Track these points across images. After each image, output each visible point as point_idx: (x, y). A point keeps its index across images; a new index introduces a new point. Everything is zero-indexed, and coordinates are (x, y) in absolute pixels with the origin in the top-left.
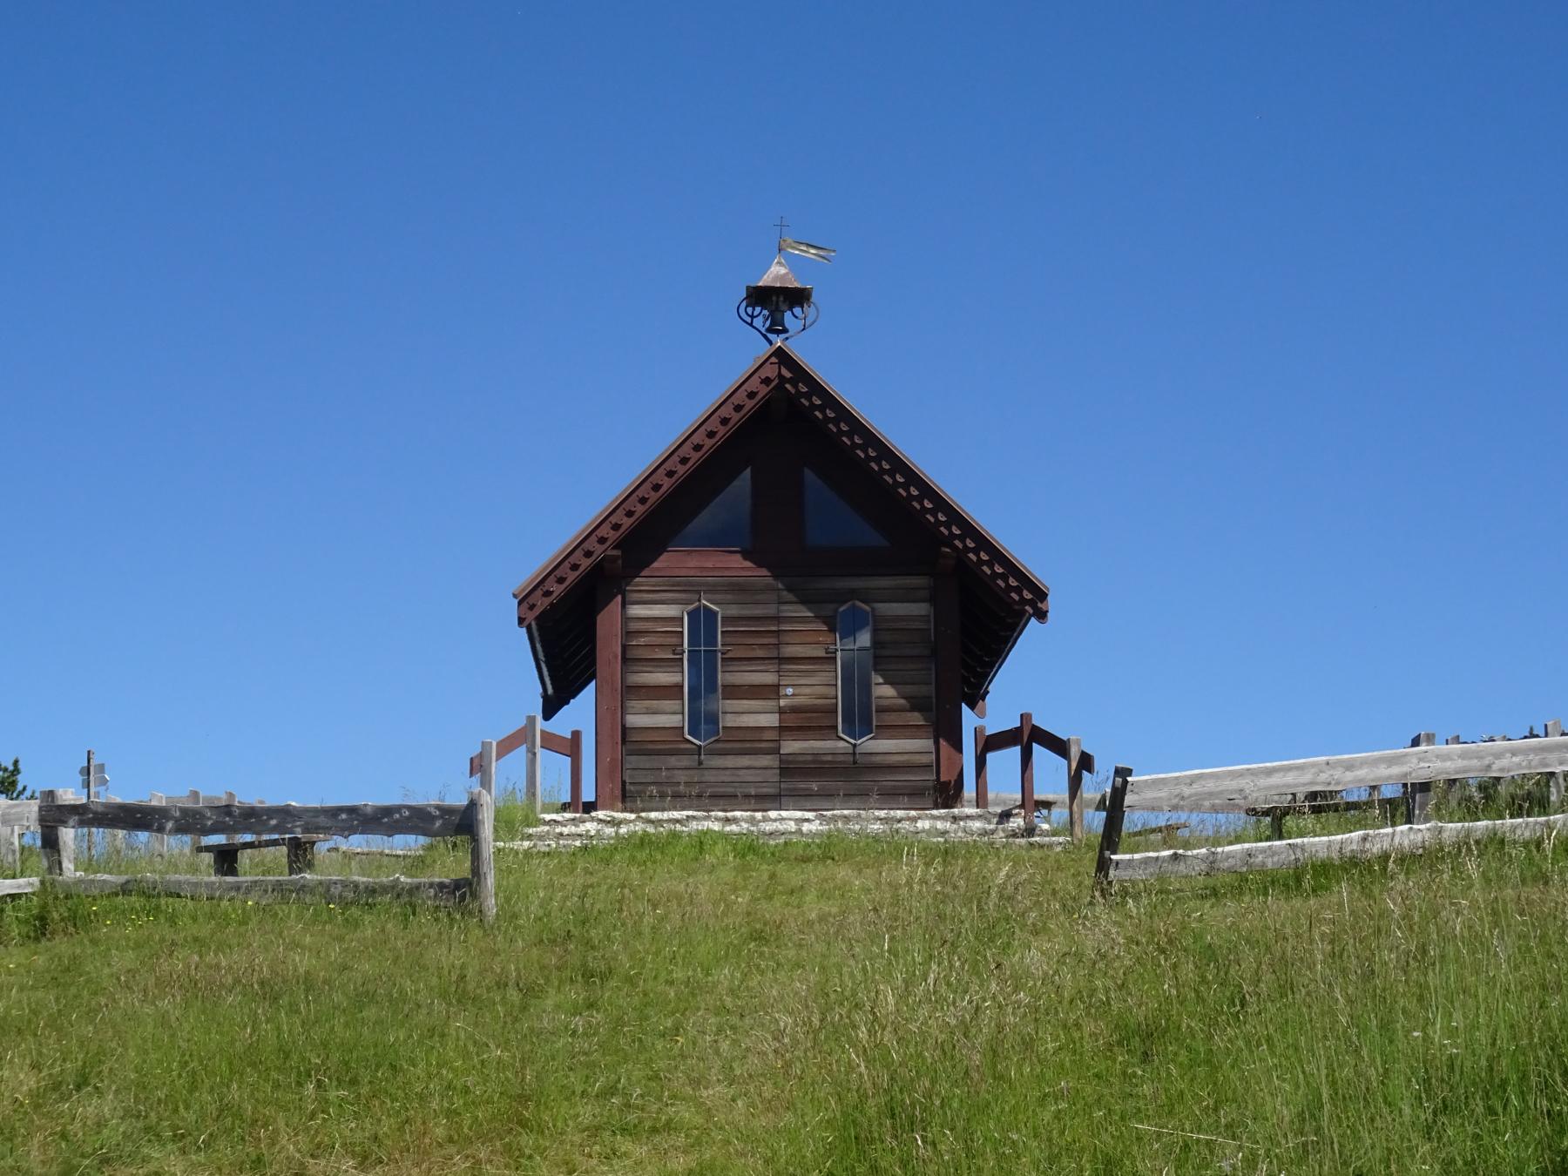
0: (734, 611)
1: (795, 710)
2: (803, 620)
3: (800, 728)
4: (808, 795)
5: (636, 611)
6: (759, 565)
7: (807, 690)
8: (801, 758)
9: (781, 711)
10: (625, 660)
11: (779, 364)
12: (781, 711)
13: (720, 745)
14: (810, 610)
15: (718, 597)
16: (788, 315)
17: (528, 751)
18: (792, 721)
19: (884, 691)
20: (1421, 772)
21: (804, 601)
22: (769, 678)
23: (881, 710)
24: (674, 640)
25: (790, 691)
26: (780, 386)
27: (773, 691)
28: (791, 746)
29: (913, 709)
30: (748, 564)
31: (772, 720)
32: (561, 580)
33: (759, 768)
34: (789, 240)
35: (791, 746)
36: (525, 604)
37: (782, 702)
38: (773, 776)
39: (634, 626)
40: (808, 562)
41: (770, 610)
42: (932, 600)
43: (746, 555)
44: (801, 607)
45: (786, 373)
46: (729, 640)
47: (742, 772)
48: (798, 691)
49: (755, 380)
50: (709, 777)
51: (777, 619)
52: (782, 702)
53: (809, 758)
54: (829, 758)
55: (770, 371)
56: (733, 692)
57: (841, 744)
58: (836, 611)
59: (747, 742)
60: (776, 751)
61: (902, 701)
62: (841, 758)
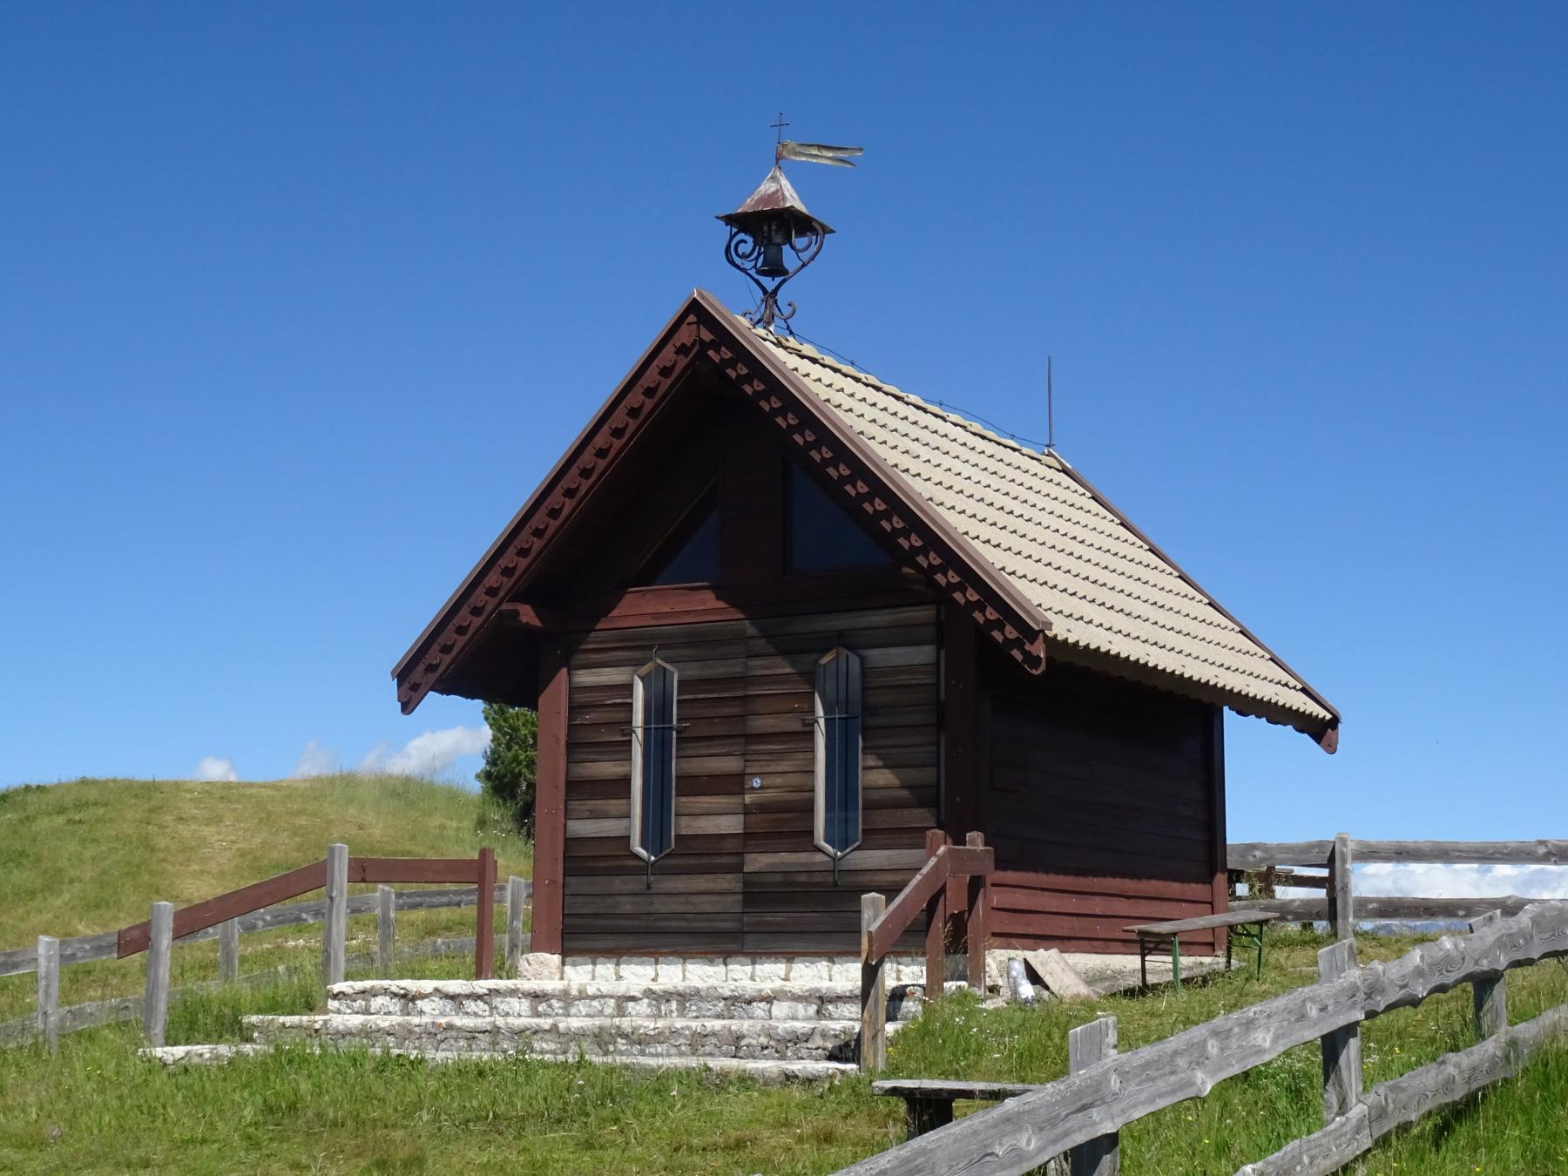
0: (694, 671)
1: (762, 808)
3: (768, 835)
4: (800, 933)
5: (585, 678)
6: (733, 603)
7: (779, 781)
8: (769, 879)
9: (747, 811)
10: (572, 746)
11: (698, 323)
12: (747, 811)
13: (673, 861)
14: (792, 664)
15: (674, 653)
16: (786, 248)
17: (1257, 724)
18: (760, 822)
19: (876, 777)
21: (785, 652)
22: (731, 764)
24: (621, 716)
25: (757, 782)
26: (702, 355)
27: (732, 784)
28: (757, 862)
29: (921, 805)
30: (722, 605)
31: (731, 824)
32: (446, 649)
33: (714, 892)
34: (791, 144)
35: (757, 862)
36: (406, 685)
37: (748, 799)
38: (733, 904)
39: (581, 698)
42: (939, 643)
43: (720, 591)
44: (778, 660)
45: (707, 336)
47: (695, 899)
48: (771, 780)
49: (669, 350)
50: (661, 905)
51: (743, 680)
52: (748, 799)
53: (778, 878)
54: (804, 878)
55: (685, 336)
56: (694, 785)
57: (819, 857)
58: (816, 662)
59: (704, 854)
60: (737, 869)
61: (905, 793)
62: (818, 878)
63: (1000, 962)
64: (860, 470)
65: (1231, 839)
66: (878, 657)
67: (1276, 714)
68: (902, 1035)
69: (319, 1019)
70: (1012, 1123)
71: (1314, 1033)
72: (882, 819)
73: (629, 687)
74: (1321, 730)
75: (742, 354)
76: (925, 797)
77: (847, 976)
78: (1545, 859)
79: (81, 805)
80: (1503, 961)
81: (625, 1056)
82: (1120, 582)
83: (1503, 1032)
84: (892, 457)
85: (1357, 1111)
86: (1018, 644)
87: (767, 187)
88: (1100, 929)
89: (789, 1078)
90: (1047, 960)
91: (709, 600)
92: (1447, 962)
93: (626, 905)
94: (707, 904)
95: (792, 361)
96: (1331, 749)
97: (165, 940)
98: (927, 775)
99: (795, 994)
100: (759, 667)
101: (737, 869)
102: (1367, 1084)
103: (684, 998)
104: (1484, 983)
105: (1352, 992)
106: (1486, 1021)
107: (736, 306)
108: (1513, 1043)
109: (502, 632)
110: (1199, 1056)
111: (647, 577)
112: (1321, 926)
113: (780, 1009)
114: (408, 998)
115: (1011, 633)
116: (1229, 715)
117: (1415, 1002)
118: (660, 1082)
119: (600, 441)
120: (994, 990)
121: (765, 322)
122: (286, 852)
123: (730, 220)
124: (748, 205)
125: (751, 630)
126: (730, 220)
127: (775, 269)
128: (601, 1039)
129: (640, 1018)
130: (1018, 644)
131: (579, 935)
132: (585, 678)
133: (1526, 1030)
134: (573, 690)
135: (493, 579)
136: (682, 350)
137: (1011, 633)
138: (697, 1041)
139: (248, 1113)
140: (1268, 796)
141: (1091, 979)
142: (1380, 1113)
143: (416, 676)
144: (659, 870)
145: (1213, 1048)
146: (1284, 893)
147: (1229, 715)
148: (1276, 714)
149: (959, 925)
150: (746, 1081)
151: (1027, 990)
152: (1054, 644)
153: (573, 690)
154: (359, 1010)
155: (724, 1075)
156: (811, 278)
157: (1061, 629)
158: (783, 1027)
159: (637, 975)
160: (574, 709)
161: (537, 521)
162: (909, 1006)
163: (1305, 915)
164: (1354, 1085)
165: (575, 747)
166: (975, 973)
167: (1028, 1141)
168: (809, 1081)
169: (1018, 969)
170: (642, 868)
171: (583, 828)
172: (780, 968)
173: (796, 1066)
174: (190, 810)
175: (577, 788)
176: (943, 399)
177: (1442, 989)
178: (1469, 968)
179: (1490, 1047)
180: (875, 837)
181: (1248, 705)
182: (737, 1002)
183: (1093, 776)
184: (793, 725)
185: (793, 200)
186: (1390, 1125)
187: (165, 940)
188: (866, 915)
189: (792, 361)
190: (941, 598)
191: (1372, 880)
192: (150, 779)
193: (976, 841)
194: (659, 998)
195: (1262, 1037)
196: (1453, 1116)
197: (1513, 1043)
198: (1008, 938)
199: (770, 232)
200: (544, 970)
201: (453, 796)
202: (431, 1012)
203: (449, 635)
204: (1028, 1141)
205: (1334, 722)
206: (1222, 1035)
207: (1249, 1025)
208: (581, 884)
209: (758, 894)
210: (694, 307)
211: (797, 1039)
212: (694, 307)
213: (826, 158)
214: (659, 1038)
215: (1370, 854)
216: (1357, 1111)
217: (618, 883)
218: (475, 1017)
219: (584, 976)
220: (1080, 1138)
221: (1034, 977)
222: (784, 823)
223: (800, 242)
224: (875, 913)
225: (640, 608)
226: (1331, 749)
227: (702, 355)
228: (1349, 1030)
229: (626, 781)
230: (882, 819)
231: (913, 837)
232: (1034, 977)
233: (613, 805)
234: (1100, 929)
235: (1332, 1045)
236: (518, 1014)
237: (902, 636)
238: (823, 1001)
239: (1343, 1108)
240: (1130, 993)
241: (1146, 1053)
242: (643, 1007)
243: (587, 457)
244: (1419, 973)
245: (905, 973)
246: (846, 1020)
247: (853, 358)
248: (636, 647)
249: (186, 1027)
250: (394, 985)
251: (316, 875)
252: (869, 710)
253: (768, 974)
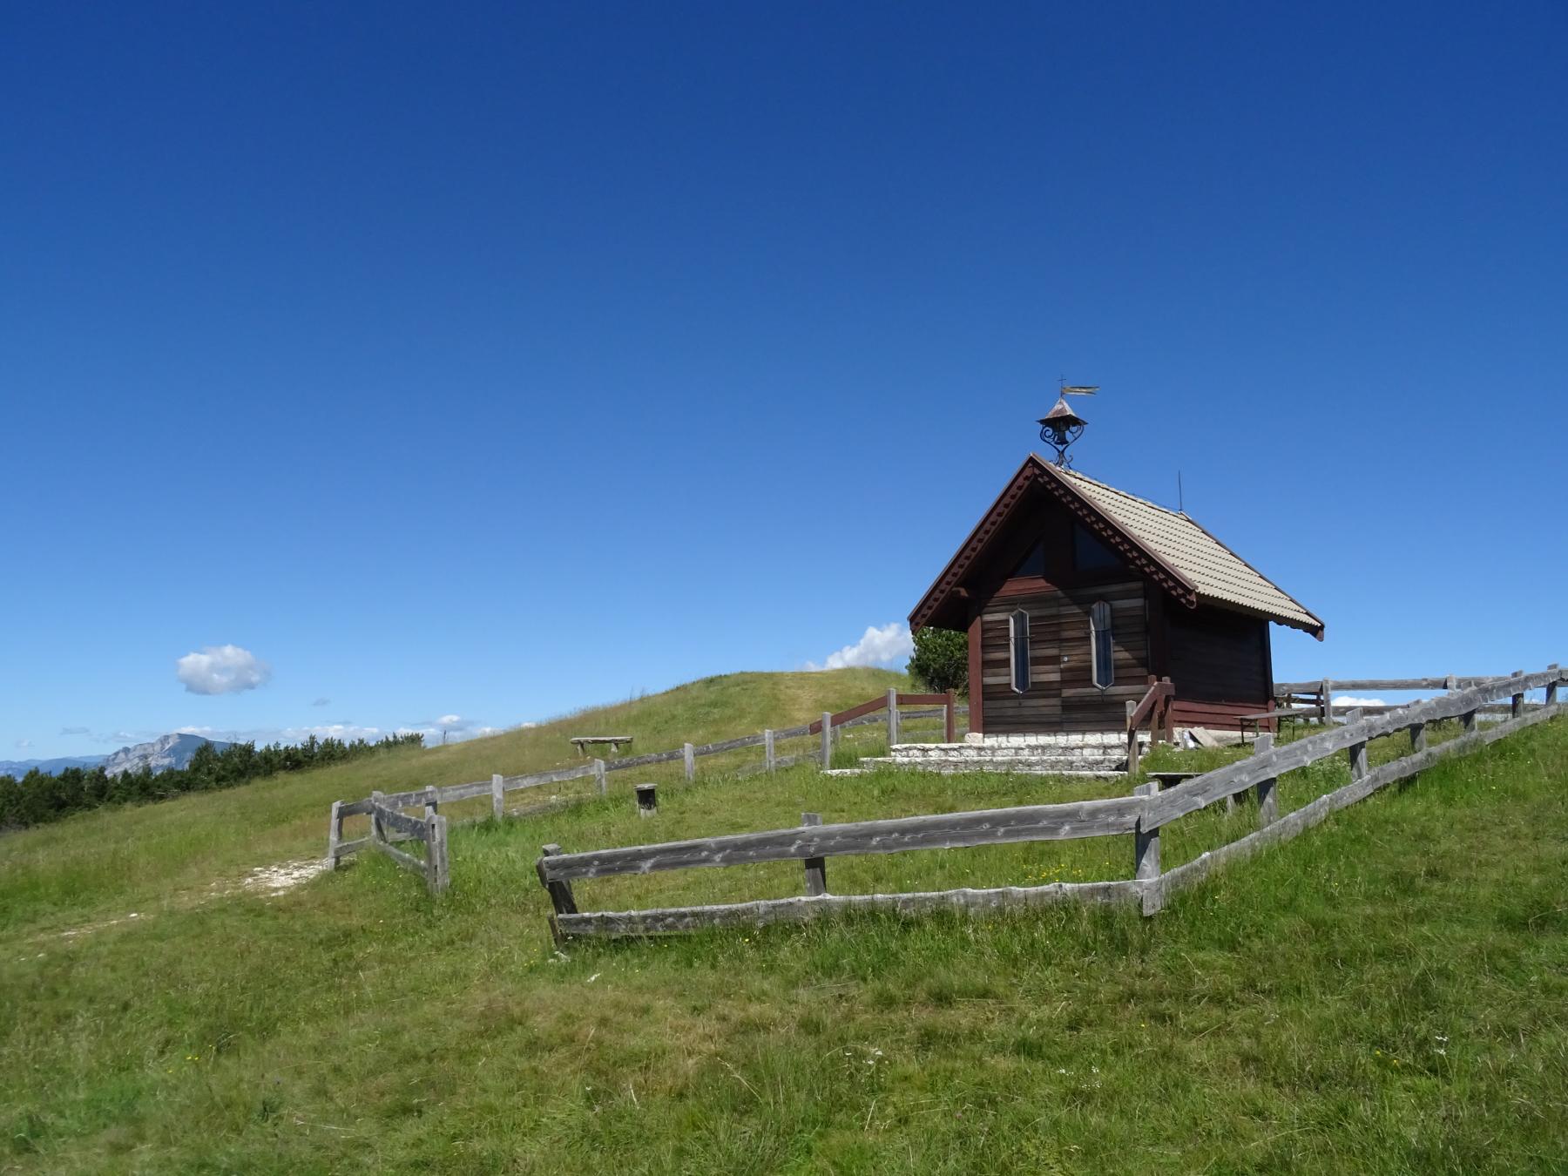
0: (1036, 613)
2: (1074, 615)
4: (1078, 722)
5: (988, 618)
9: (1062, 671)
10: (983, 646)
12: (1062, 671)
19: (1120, 655)
20: (639, 976)
22: (1054, 652)
23: (1117, 668)
26: (1035, 480)
27: (1055, 660)
28: (1067, 692)
31: (1055, 677)
35: (1067, 692)
38: (1058, 710)
40: (1045, 594)
41: (1053, 611)
46: (905, 709)
49: (1021, 479)
50: (1026, 712)
55: (1028, 472)
56: (1038, 661)
60: (1059, 696)
63: (1179, 733)
64: (1109, 525)
65: (1276, 680)
66: (1119, 604)
67: (1295, 624)
68: (1144, 760)
69: (887, 759)
70: (1239, 770)
71: (1348, 745)
72: (1122, 673)
73: (1007, 621)
74: (1316, 631)
75: (1053, 479)
76: (1143, 663)
77: (1124, 737)
78: (1426, 687)
79: (745, 682)
80: (1424, 720)
81: (1021, 770)
82: (1221, 568)
83: (1425, 750)
84: (1120, 519)
85: (1366, 777)
86: (1183, 596)
87: (1058, 407)
88: (1219, 719)
89: (1098, 777)
90: (1198, 731)
91: (1042, 583)
92: (1400, 719)
93: (1010, 712)
94: (1046, 711)
95: (1074, 480)
96: (1321, 639)
97: (828, 728)
98: (1143, 654)
99: (1093, 747)
100: (1065, 610)
101: (1059, 696)
102: (1370, 767)
103: (1044, 748)
104: (1415, 729)
105: (1363, 729)
106: (1417, 746)
107: (1047, 456)
108: (1430, 754)
109: (953, 598)
110: (1306, 752)
111: (1012, 575)
112: (1314, 720)
113: (1086, 752)
114: (925, 750)
115: (1180, 591)
116: (1272, 624)
117: (1388, 735)
118: (1043, 780)
119: (992, 519)
120: (1177, 744)
121: (1059, 464)
122: (872, 691)
123: (1042, 422)
124: (1050, 415)
125: (1059, 593)
126: (1042, 422)
127: (1063, 441)
128: (1011, 764)
129: (1025, 755)
130: (1183, 596)
131: (990, 725)
132: (988, 618)
133: (1434, 749)
134: (983, 623)
135: (949, 578)
136: (1027, 478)
137: (1180, 591)
138: (1053, 765)
139: (876, 793)
140: (1291, 661)
141: (1219, 740)
142: (1376, 779)
143: (918, 619)
144: (1024, 697)
145: (1310, 747)
146: (1294, 705)
147: (1272, 624)
148: (1295, 624)
149: (1162, 717)
150: (1080, 779)
151: (1191, 744)
152: (1201, 596)
153: (983, 623)
154: (903, 755)
155: (1070, 777)
156: (1078, 444)
157: (1202, 589)
158: (1091, 758)
159: (1017, 740)
160: (984, 631)
161: (967, 553)
162: (1145, 749)
163: (1306, 715)
164: (1364, 768)
165: (985, 647)
166: (1170, 737)
167: (1245, 778)
168: (1106, 779)
169: (1187, 735)
170: (1017, 696)
171: (989, 680)
172: (1080, 737)
173: (1102, 773)
174: (791, 684)
175: (987, 664)
176: (1134, 493)
177: (1398, 730)
178: (1410, 722)
179: (1418, 757)
180: (1119, 681)
181: (1281, 620)
182: (1067, 749)
183: (1212, 654)
184: (1080, 634)
185: (1070, 412)
186: (1381, 783)
187: (828, 728)
188: (1129, 710)
189: (1074, 480)
190: (1146, 578)
191: (1340, 700)
192: (637, 695)
193: (1167, 680)
194: (1032, 748)
195: (1329, 745)
196: (1406, 783)
197: (1430, 754)
198: (1181, 723)
199: (1060, 426)
200: (975, 738)
201: (898, 676)
202: (934, 756)
203: (930, 602)
204: (1245, 778)
205: (1322, 627)
206: (1313, 743)
207: (1323, 740)
208: (989, 703)
209: (1069, 706)
210: (1031, 460)
211: (1097, 763)
212: (1031, 460)
213: (1083, 393)
214: (1037, 763)
215: (1339, 687)
216: (1366, 777)
217: (1007, 703)
218: (954, 757)
219: (991, 741)
220: (1263, 778)
221: (1193, 738)
222: (1079, 676)
223: (1073, 429)
224: (1132, 710)
225: (1011, 588)
226: (1321, 639)
227: (1035, 480)
228: (1362, 745)
229: (1008, 660)
230: (1122, 673)
231: (1143, 680)
232: (1193, 738)
233: (1003, 670)
234: (1219, 719)
235: (1354, 752)
236: (972, 755)
237: (1127, 595)
238: (1106, 748)
239: (1360, 776)
240: (1238, 746)
241: (1285, 748)
242: (1026, 752)
243: (987, 526)
244: (1389, 723)
245: (1143, 737)
246: (1118, 755)
247: (1097, 477)
248: (1010, 604)
249: (838, 762)
250: (919, 745)
251: (882, 702)
252: (1114, 626)
253: (1075, 739)
